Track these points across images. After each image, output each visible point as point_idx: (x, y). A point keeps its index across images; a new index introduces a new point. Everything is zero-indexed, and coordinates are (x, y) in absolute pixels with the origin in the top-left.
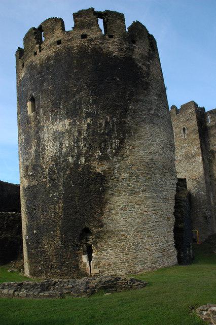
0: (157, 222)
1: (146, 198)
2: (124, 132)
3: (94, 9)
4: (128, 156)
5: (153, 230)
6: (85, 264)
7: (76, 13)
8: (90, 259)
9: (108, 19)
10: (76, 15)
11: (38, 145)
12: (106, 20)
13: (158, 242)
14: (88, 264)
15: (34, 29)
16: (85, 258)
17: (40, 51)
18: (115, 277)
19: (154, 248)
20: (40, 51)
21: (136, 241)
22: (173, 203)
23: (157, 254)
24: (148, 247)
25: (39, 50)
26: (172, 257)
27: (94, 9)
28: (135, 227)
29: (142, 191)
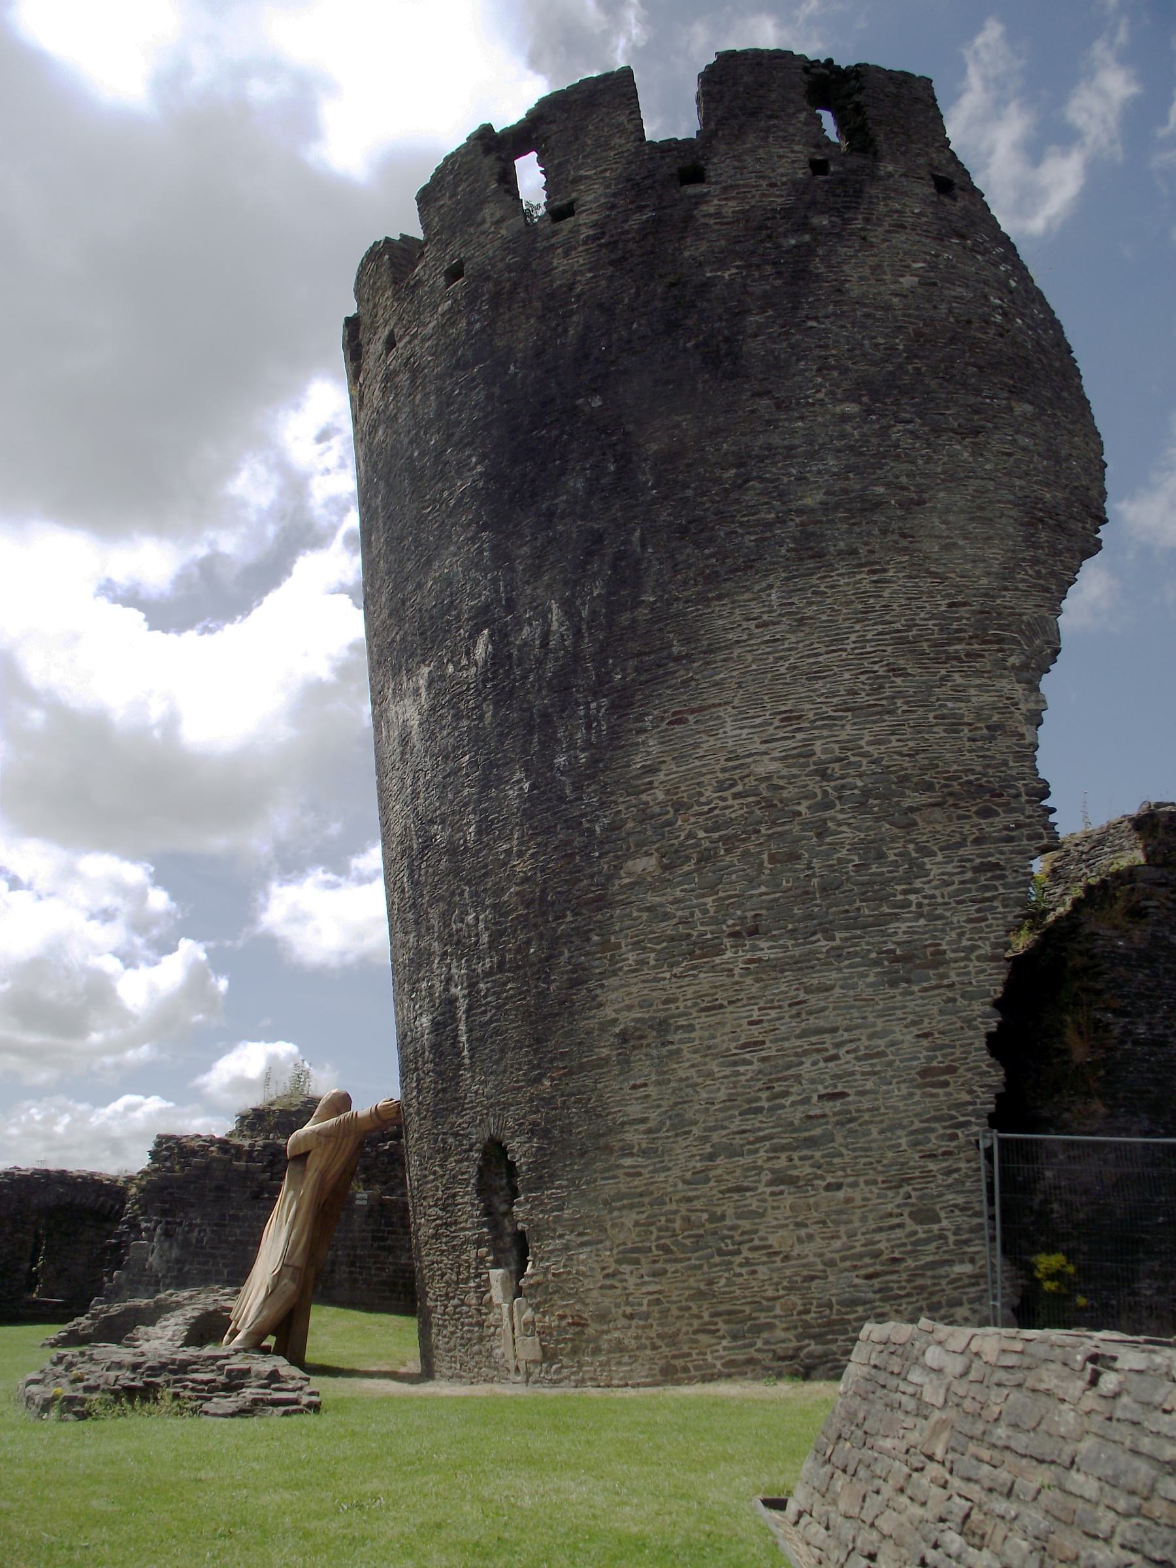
4: (652, 770)
19: (809, 1248)
29: (735, 935)
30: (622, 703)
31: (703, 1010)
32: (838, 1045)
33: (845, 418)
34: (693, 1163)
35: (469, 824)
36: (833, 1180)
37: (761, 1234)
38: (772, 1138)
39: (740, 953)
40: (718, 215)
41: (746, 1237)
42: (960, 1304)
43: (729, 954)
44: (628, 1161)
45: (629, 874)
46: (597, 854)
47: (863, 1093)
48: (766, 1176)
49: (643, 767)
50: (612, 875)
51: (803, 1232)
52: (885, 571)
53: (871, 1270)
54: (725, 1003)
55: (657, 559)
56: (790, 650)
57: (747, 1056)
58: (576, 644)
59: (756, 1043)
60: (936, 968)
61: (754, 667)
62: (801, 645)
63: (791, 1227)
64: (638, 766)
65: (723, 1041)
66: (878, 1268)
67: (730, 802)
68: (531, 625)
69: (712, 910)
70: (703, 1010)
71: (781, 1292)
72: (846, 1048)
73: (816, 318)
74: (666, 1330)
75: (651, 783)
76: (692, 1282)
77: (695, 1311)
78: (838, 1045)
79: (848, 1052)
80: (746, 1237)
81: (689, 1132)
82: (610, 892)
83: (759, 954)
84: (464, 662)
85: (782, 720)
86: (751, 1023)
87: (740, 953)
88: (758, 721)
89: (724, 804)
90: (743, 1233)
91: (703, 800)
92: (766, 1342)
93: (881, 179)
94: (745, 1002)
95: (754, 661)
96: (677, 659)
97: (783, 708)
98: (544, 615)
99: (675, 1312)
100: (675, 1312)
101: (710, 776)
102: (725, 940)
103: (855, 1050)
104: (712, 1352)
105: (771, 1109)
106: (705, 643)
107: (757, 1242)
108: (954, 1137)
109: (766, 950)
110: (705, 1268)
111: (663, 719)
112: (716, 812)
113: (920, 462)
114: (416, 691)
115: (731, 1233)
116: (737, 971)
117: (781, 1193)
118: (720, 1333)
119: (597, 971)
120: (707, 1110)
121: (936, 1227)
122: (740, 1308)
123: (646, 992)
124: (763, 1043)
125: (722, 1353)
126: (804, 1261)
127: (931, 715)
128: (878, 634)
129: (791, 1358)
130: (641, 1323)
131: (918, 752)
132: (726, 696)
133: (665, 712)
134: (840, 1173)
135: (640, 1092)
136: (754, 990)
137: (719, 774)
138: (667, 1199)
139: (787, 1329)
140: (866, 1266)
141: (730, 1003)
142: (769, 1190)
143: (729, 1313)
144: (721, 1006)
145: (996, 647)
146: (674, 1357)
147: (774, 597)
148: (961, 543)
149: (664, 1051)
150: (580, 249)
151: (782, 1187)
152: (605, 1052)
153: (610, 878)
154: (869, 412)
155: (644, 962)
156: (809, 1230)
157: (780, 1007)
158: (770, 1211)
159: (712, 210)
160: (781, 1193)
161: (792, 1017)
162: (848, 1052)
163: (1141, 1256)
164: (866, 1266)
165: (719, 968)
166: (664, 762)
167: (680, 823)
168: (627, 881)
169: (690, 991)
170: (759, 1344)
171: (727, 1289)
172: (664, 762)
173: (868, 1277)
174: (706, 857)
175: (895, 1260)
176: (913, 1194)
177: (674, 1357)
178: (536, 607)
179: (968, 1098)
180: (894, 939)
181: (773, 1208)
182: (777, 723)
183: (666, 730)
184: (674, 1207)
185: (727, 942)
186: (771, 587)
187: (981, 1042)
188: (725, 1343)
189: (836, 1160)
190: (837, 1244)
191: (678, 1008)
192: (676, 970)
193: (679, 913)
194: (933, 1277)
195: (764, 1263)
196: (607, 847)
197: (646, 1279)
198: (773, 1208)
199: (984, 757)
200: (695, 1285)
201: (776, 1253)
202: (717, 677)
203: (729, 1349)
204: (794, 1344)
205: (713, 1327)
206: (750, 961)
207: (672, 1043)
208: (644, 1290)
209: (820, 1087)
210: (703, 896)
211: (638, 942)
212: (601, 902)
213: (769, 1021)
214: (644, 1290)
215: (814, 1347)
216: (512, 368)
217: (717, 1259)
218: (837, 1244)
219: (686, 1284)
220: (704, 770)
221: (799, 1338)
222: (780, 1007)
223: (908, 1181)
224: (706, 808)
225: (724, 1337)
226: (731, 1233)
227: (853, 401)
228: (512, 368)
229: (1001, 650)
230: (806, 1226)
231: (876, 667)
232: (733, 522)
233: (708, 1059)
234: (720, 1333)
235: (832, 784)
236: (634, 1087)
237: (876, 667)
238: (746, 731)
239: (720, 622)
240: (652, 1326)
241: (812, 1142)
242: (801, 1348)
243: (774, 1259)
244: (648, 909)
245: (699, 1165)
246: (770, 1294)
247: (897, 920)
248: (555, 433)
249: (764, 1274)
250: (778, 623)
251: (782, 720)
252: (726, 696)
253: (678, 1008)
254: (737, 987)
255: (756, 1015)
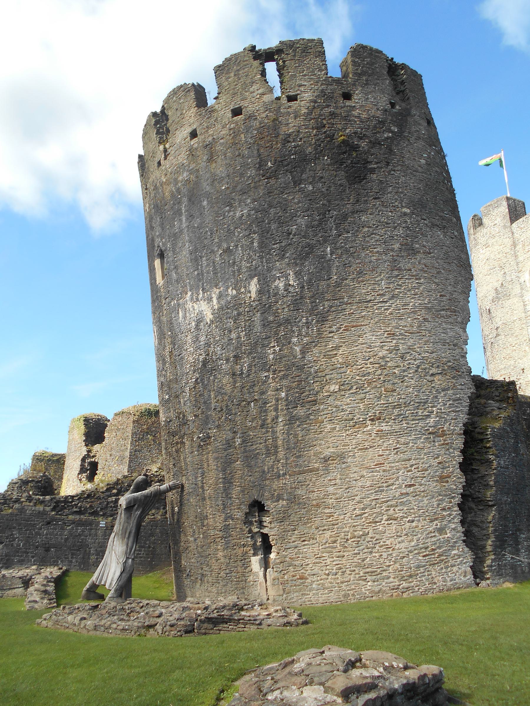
0: (410, 486)
1: (381, 434)
2: (464, 694)
3: (254, 47)
4: (337, 348)
5: (402, 503)
6: (256, 574)
7: (219, 66)
8: (266, 564)
9: (284, 62)
10: (219, 70)
11: (173, 343)
12: (281, 62)
13: (412, 533)
14: (261, 574)
15: (154, 114)
16: (255, 562)
17: (165, 158)
18: (138, 413)
19: (403, 545)
20: (165, 158)
21: (359, 528)
22: (459, 442)
23: (412, 561)
24: (388, 542)
25: (163, 156)
26: (455, 569)
27: (254, 47)
28: (357, 498)
29: (372, 420)
30: (323, 319)
31: (359, 449)
32: (412, 466)
33: (405, 214)
34: (355, 512)
35: (245, 362)
36: (411, 519)
37: (384, 540)
38: (388, 502)
39: (374, 427)
40: (358, 117)
41: (378, 542)
42: (455, 566)
43: (369, 427)
44: (327, 511)
45: (327, 392)
46: (312, 382)
47: (421, 485)
48: (385, 517)
49: (332, 347)
50: (319, 391)
51: (400, 539)
52: (420, 279)
53: (425, 554)
54: (369, 447)
55: (337, 261)
56: (389, 306)
57: (378, 469)
58: (301, 292)
59: (381, 464)
60: (443, 437)
61: (376, 311)
62: (393, 305)
63: (395, 537)
64: (330, 346)
65: (368, 463)
66: (427, 553)
67: (368, 366)
68: (279, 279)
69: (363, 409)
70: (359, 449)
71: (392, 563)
72: (414, 467)
73: (394, 170)
74: (344, 579)
75: (336, 354)
76: (355, 560)
77: (357, 572)
78: (412, 466)
79: (415, 468)
80: (378, 542)
81: (354, 499)
82: (319, 398)
83: (382, 428)
84: (243, 290)
85: (388, 334)
86: (379, 456)
87: (374, 427)
88: (379, 333)
89: (366, 366)
90: (377, 540)
91: (358, 363)
92: (387, 583)
93: (412, 116)
94: (376, 447)
95: (376, 309)
96: (347, 304)
97: (388, 330)
98: (287, 277)
99: (348, 572)
100: (348, 572)
101: (360, 354)
102: (368, 421)
103: (418, 468)
104: (364, 588)
105: (387, 490)
106: (358, 299)
107: (382, 543)
108: (451, 502)
109: (385, 427)
110: (361, 553)
111: (340, 328)
112: (363, 369)
113: (429, 237)
114: (210, 299)
115: (371, 540)
116: (373, 435)
117: (391, 524)
118: (367, 580)
119: (313, 431)
120: (362, 490)
121: (446, 536)
122: (376, 570)
123: (335, 441)
124: (384, 464)
125: (369, 588)
126: (400, 551)
127: (437, 338)
128: (420, 304)
129: (397, 589)
130: (333, 577)
131: (433, 352)
132: (366, 322)
133: (341, 325)
134: (413, 516)
135: (333, 482)
136: (380, 442)
137: (364, 354)
138: (345, 526)
139: (394, 578)
140: (423, 552)
141: (370, 447)
142: (386, 522)
143: (372, 572)
144: (367, 449)
145: (454, 314)
146: (348, 590)
147: (383, 284)
148: (443, 271)
149: (343, 466)
150: (302, 117)
151: (391, 521)
152: (316, 465)
153: (318, 392)
154: (413, 213)
155: (335, 428)
156: (402, 538)
157: (390, 450)
158: (387, 531)
159: (356, 114)
160: (391, 524)
161: (395, 454)
162: (415, 468)
163: (506, 546)
164: (423, 552)
165: (366, 433)
166: (342, 346)
167: (348, 372)
168: (326, 394)
169: (354, 441)
170: (384, 584)
171: (370, 562)
172: (342, 346)
173: (424, 556)
174: (361, 388)
175: (433, 550)
176: (438, 524)
177: (348, 590)
178: (282, 273)
179: (455, 487)
180: (429, 425)
181: (388, 530)
182: (386, 335)
183: (342, 333)
184: (347, 529)
185: (369, 422)
186: (382, 280)
187: (457, 466)
188: (369, 584)
189: (411, 511)
190: (413, 544)
191: (349, 448)
192: (347, 433)
193: (349, 409)
194: (446, 556)
195: (385, 552)
196: (316, 379)
197: (335, 558)
198: (388, 530)
199: (453, 356)
200: (357, 561)
201: (390, 548)
202: (363, 314)
203: (372, 586)
204: (397, 583)
205: (365, 578)
206: (378, 431)
207: (347, 463)
208: (334, 563)
209: (405, 482)
210: (358, 403)
211: (331, 420)
212: (315, 402)
213: (386, 455)
214: (334, 563)
215: (405, 584)
216: (269, 164)
217: (366, 550)
218: (413, 544)
219: (352, 561)
220: (358, 351)
221: (400, 580)
222: (390, 450)
223: (436, 519)
224: (359, 367)
225: (369, 582)
226: (371, 540)
227: (408, 208)
228: (269, 164)
229: (456, 315)
230: (401, 537)
231: (419, 317)
232: (367, 250)
233: (362, 470)
234: (367, 580)
235: (406, 362)
236: (330, 480)
237: (419, 317)
238: (374, 337)
239: (363, 291)
240: (338, 578)
241: (402, 503)
242: (400, 585)
243: (389, 550)
244: (336, 407)
245: (358, 512)
246: (387, 564)
247: (430, 418)
248: (290, 198)
249: (385, 556)
250: (385, 295)
251: (388, 334)
252: (366, 322)
253: (349, 448)
254: (373, 441)
255: (381, 453)
